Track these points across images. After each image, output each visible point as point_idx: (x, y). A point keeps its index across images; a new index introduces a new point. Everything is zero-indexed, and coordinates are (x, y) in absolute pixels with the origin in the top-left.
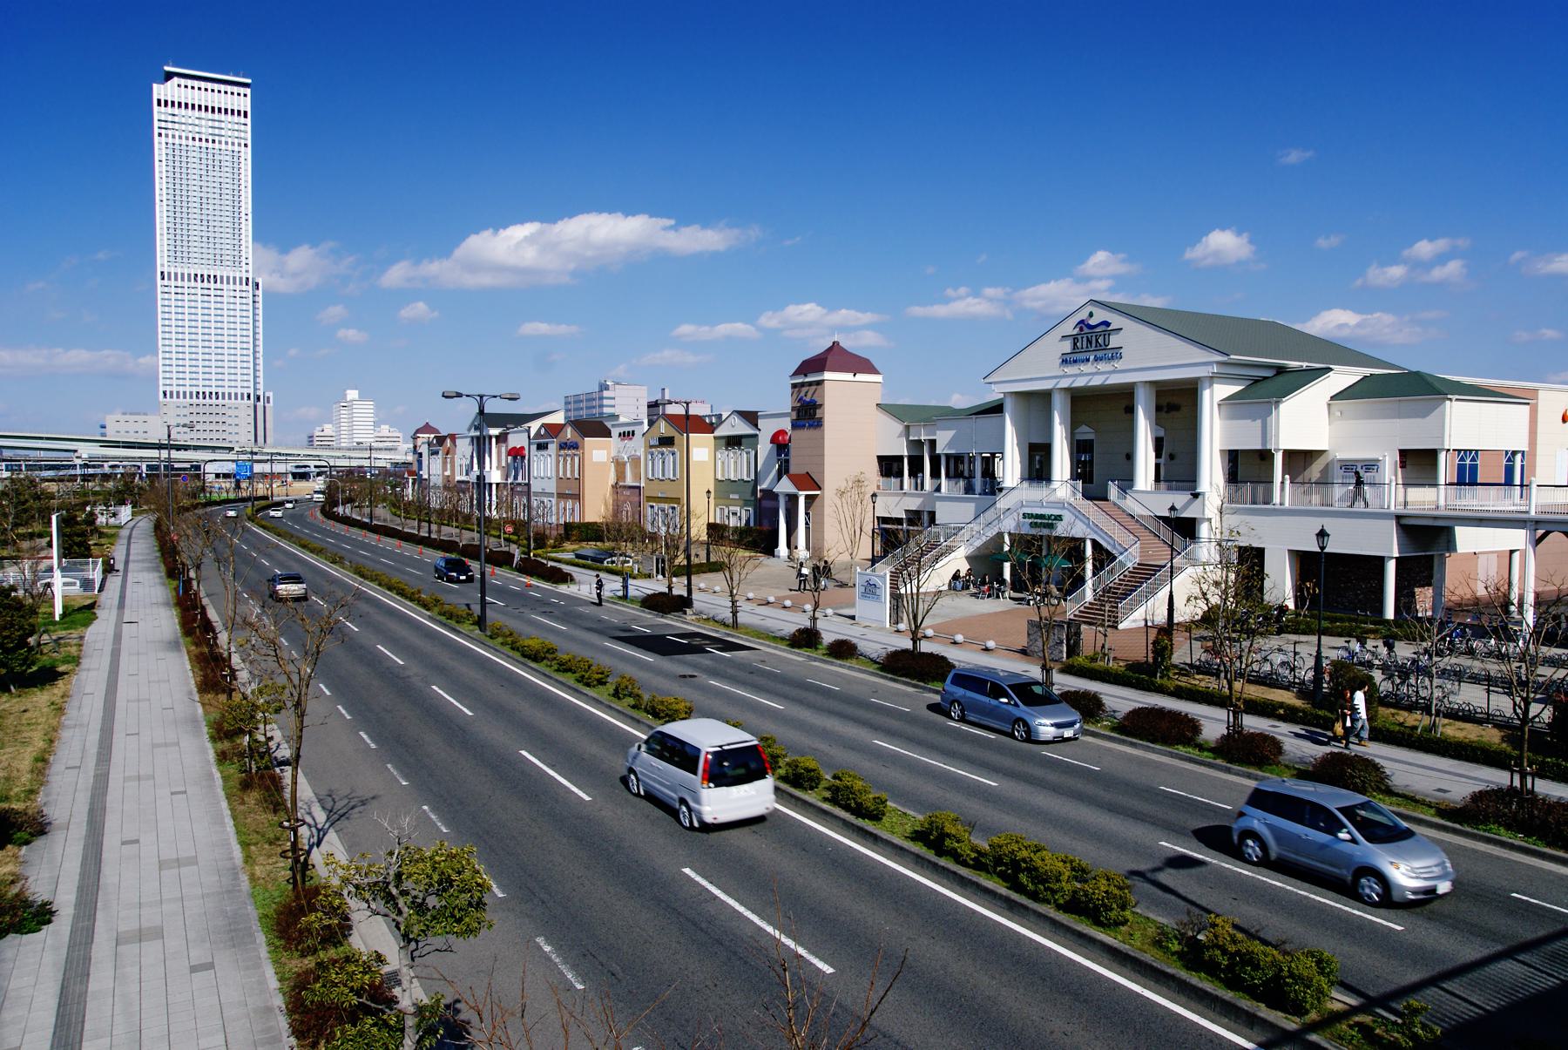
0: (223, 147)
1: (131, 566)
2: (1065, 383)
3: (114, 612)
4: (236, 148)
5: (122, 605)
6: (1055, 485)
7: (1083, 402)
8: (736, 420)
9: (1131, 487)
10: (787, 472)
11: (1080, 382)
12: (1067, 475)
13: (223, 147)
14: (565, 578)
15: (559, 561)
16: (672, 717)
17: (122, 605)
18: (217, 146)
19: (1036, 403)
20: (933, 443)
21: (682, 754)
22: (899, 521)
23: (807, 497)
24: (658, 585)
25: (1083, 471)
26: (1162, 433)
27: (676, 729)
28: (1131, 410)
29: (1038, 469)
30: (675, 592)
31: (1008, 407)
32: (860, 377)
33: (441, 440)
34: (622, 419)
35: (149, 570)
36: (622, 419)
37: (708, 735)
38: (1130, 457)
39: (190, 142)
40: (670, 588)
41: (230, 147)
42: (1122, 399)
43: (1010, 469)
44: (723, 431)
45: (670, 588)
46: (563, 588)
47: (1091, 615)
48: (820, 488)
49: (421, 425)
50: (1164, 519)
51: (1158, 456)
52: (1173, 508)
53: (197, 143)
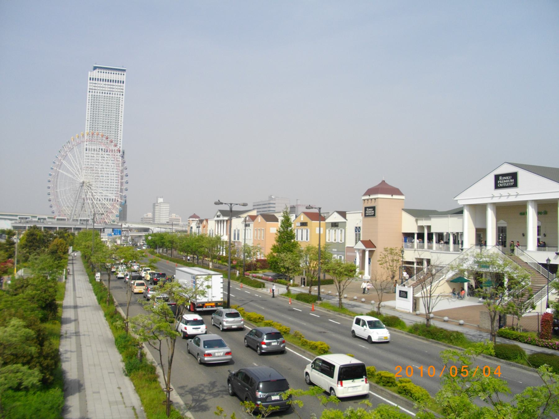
0: (114, 96)
1: (75, 273)
2: (496, 200)
3: (72, 292)
4: (119, 96)
5: (74, 289)
6: (488, 248)
7: (502, 209)
8: (336, 214)
9: (526, 249)
10: (359, 240)
11: (504, 200)
12: (494, 243)
13: (114, 96)
14: (262, 286)
15: (256, 277)
16: (325, 352)
17: (74, 289)
18: (111, 95)
19: (479, 210)
20: (429, 227)
21: (327, 369)
22: (412, 263)
23: (370, 251)
24: (304, 290)
25: (502, 241)
26: (540, 224)
27: (327, 358)
28: (524, 214)
29: (481, 240)
30: (312, 293)
31: (466, 213)
32: (395, 197)
33: (201, 221)
34: (213, 229)
35: (82, 274)
36: (213, 229)
37: (339, 360)
38: (524, 235)
39: (101, 94)
40: (310, 292)
41: (116, 96)
42: (519, 209)
43: (469, 239)
44: (330, 220)
45: (310, 292)
46: (260, 290)
47: (509, 309)
48: (375, 247)
49: (192, 214)
50: (543, 265)
51: (538, 234)
52: (548, 260)
53: (104, 95)
